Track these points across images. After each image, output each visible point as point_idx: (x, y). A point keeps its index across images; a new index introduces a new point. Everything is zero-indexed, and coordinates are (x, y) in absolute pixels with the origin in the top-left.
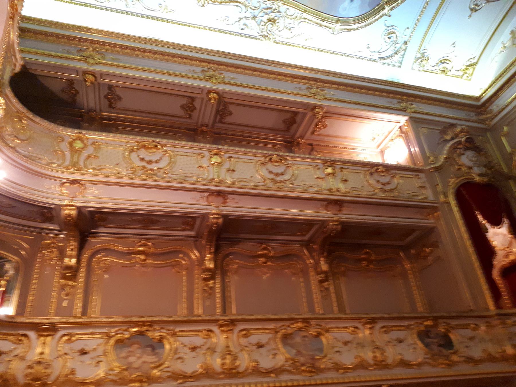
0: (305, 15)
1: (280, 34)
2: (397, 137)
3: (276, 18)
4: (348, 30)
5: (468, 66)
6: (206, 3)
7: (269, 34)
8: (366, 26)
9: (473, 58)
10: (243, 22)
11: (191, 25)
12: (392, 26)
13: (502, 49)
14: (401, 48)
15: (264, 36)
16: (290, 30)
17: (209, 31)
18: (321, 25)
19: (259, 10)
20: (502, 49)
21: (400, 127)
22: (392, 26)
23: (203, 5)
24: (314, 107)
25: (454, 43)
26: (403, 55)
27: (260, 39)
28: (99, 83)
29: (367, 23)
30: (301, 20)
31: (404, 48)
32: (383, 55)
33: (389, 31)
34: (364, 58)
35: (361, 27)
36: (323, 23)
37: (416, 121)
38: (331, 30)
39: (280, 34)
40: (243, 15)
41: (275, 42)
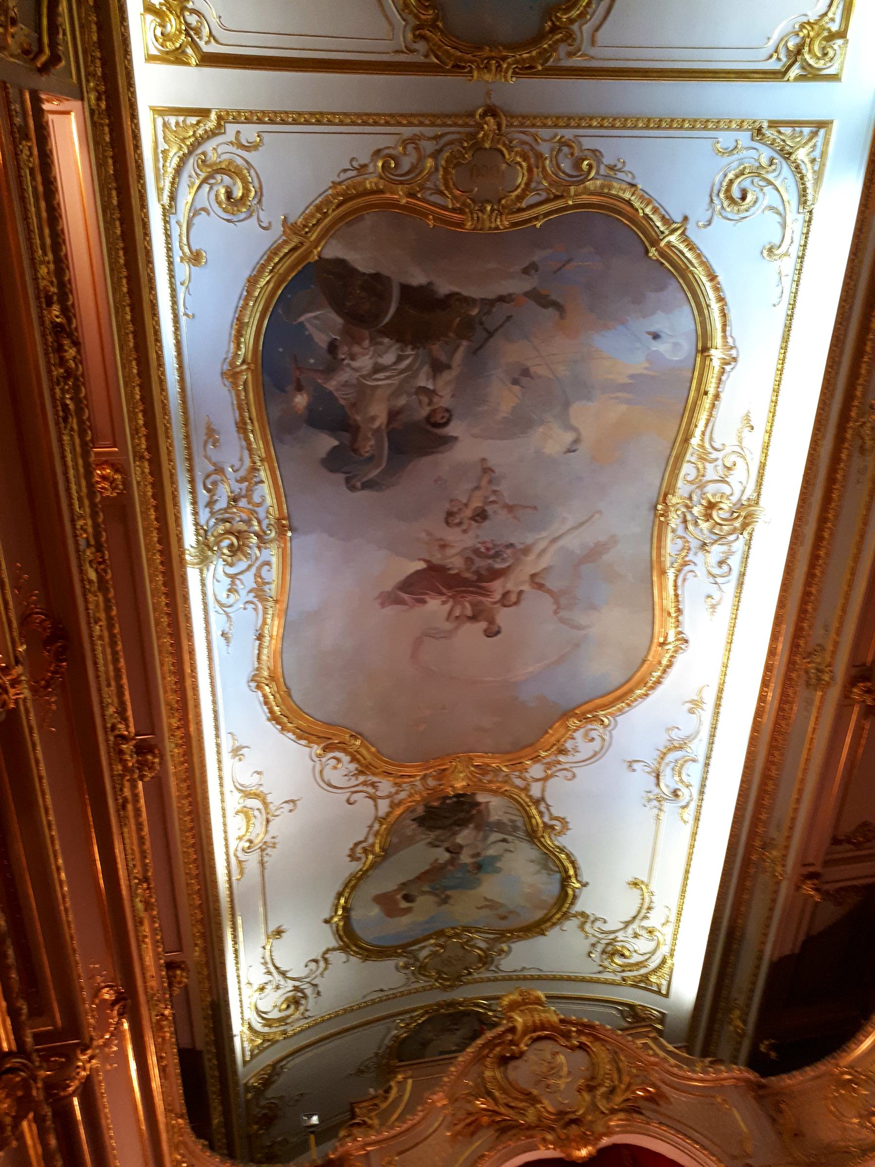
3: (704, 502)
4: (724, 325)
8: (712, 277)
11: (776, 391)
16: (729, 469)
18: (717, 397)
27: (751, 534)
28: (826, 863)
30: (707, 445)
33: (726, 203)
34: (694, 834)
35: (717, 289)
36: (712, 391)
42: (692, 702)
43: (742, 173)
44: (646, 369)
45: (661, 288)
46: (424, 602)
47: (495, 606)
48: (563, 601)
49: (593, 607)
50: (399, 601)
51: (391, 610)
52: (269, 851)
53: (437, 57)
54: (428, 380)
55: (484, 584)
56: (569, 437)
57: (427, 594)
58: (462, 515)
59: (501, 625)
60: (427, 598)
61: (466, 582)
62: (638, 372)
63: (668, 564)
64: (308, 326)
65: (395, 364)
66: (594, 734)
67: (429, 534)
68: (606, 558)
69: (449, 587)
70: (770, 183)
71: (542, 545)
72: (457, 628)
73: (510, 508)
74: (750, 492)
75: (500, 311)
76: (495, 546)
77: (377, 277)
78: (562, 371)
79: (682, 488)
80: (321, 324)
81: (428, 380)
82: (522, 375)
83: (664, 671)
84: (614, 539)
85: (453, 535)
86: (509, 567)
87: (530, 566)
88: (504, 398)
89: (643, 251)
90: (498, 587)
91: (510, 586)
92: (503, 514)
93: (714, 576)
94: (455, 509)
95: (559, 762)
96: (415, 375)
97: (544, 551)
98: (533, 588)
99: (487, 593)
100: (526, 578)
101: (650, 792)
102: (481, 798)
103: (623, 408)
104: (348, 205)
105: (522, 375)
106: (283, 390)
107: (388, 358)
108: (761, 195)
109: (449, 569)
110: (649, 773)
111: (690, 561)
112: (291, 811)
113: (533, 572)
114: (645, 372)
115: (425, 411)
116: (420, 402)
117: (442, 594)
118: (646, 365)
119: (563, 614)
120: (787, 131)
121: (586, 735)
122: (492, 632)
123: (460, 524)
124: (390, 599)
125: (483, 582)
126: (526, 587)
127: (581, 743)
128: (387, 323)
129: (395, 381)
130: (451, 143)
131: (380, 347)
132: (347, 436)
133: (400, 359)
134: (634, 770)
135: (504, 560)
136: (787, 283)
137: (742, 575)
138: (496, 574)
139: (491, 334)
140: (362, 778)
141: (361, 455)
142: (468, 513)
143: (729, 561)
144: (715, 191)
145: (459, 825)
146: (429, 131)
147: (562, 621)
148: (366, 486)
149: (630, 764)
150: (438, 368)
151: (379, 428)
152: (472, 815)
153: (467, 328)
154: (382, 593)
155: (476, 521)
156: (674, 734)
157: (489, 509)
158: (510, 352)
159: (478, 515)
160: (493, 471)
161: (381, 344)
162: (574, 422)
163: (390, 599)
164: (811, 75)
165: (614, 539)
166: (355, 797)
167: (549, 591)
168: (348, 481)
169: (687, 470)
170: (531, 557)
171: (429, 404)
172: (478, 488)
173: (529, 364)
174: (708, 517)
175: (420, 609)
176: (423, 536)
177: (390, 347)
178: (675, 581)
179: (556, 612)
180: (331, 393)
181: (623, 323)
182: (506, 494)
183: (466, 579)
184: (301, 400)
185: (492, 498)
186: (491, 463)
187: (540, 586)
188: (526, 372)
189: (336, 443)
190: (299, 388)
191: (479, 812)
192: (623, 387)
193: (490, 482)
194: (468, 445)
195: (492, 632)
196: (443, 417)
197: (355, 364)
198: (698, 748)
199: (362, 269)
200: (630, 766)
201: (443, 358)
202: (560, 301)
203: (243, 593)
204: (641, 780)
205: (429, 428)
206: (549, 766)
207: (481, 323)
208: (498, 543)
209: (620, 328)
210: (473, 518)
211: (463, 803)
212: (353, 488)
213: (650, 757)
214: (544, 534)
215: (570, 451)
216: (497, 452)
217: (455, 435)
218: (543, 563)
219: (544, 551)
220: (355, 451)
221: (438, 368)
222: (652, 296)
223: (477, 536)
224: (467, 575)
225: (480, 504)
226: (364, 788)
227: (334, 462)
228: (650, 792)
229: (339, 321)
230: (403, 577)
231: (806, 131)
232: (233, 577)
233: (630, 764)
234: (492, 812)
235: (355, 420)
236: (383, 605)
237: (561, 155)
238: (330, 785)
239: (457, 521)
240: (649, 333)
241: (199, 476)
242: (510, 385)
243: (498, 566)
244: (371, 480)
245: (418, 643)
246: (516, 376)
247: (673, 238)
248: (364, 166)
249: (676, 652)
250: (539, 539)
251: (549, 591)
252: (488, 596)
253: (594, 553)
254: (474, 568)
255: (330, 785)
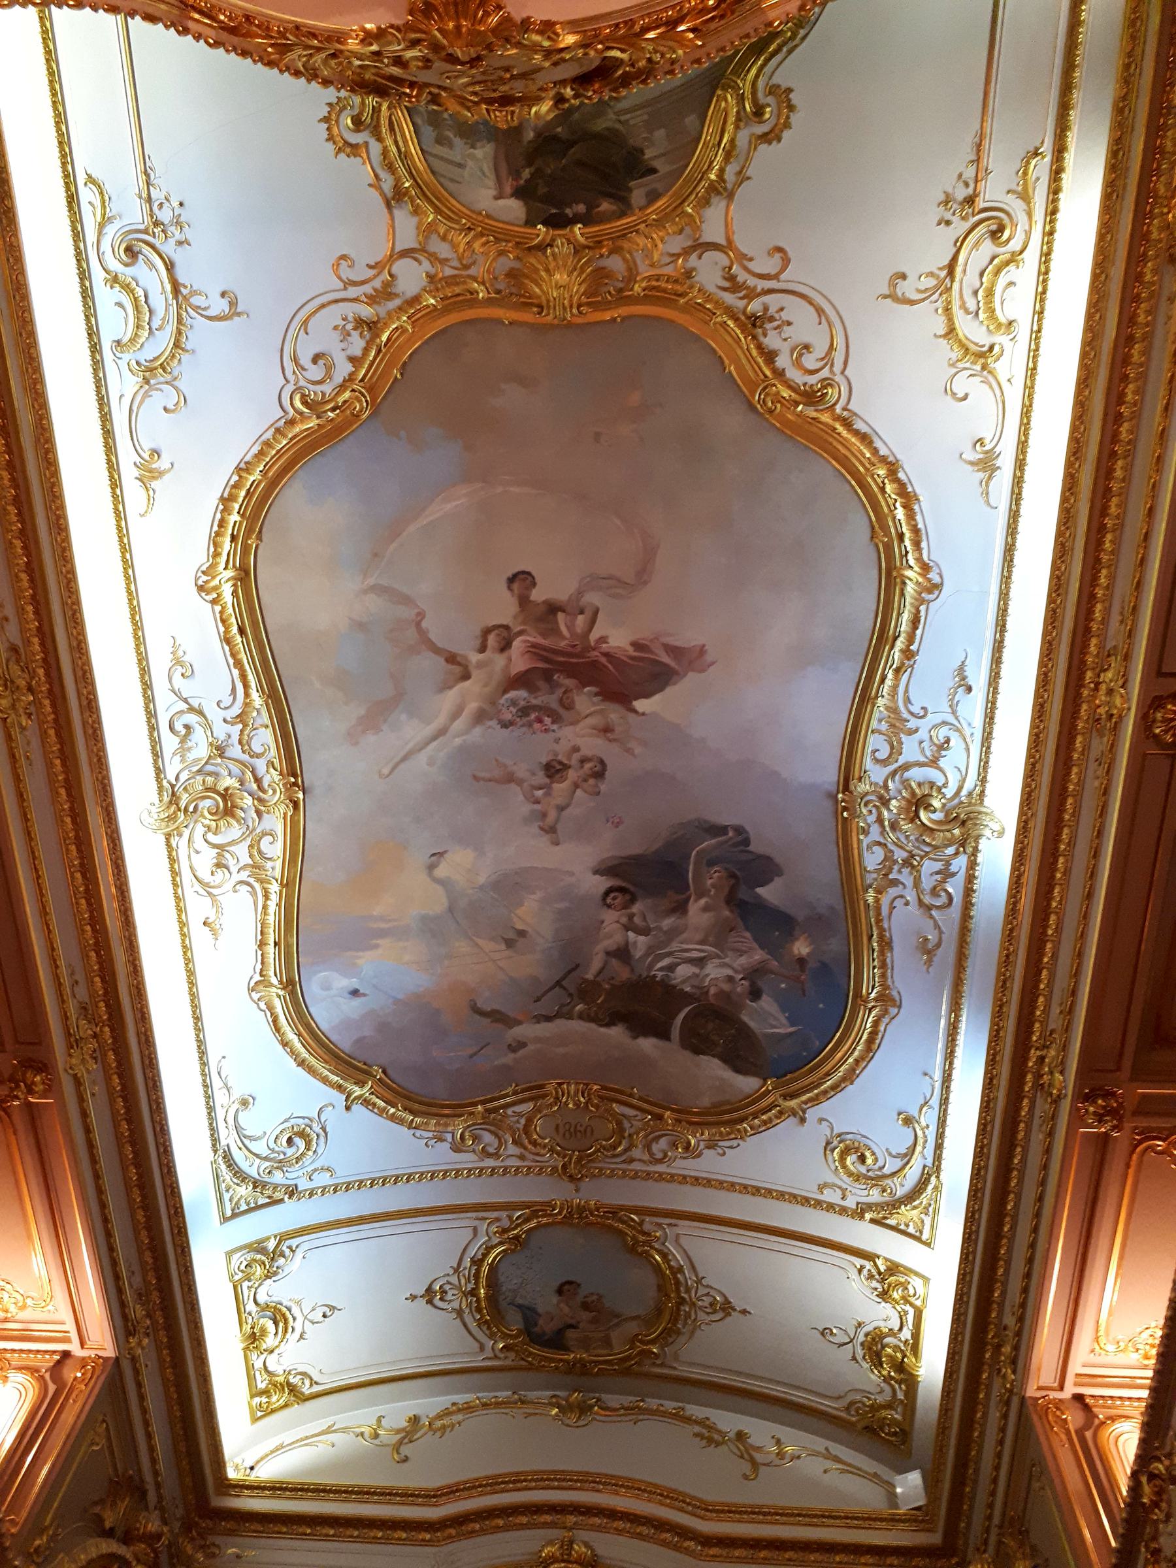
0: (274, 888)
1: (199, 843)
2: (33, 1370)
5: (289, 1384)
6: (209, 598)
7: (186, 810)
8: (301, 1063)
9: (313, 1383)
10: (192, 719)
12: (324, 1129)
13: (367, 1430)
14: (276, 1187)
15: (174, 798)
17: (129, 628)
18: (262, 944)
19: (245, 757)
20: (367, 1430)
21: (66, 1355)
22: (324, 1129)
23: (201, 589)
24: (44, 1066)
25: (333, 1308)
26: (258, 1207)
27: (160, 789)
29: (312, 1060)
30: (257, 886)
31: (278, 1195)
32: (239, 1156)
35: (293, 1053)
37: (115, 1379)
38: (257, 978)
39: (199, 843)
40: (215, 715)
41: (168, 837)
42: (159, 474)
43: (298, 1159)
44: (360, 957)
45: (359, 1041)
46: (636, 645)
47: (519, 629)
48: (411, 634)
49: (360, 626)
50: (675, 651)
51: (688, 638)
52: (961, 193)
53: (633, 1220)
54: (635, 943)
55: (541, 665)
56: (442, 871)
57: (632, 658)
58: (581, 772)
59: (507, 594)
60: (631, 651)
61: (570, 671)
62: (369, 953)
63: (264, 712)
64: (784, 1021)
65: (679, 964)
66: (315, 372)
67: (629, 751)
68: (357, 711)
69: (594, 664)
70: (266, 1159)
71: (459, 724)
72: (580, 593)
73: (510, 779)
74: (181, 844)
75: (548, 1005)
76: (530, 725)
77: (697, 1051)
78: (463, 946)
79: (275, 822)
80: (767, 1018)
81: (635, 943)
82: (514, 939)
83: (222, 523)
84: (352, 737)
85: (593, 745)
86: (505, 691)
87: (472, 692)
88: (532, 913)
89: (389, 1071)
90: (518, 660)
91: (500, 661)
92: (521, 771)
93: (192, 709)
94: (592, 781)
95: (372, 300)
96: (650, 950)
97: (455, 716)
98: (465, 658)
99: (534, 650)
100: (475, 673)
101: (180, 243)
102: (513, 209)
103: (377, 911)
104: (729, 1119)
105: (514, 939)
106: (824, 965)
107: (684, 971)
108: (272, 1145)
109: (596, 694)
110: (194, 293)
111: (236, 723)
112: (903, 277)
113: (467, 683)
114: (361, 954)
115: (636, 908)
116: (644, 919)
117: (606, 655)
118: (359, 962)
119: (408, 613)
120: (261, 1201)
121: (329, 368)
122: (521, 580)
123: (583, 761)
124: (690, 659)
125: (546, 669)
126: (474, 657)
127: (333, 342)
128: (687, 1006)
129: (675, 946)
130: (614, 1156)
131: (696, 983)
132: (743, 894)
133: (671, 968)
134: (223, 294)
135: (514, 703)
136: (217, 1083)
137: (153, 728)
138: (521, 681)
139: (558, 983)
140: (755, 306)
141: (726, 869)
142: (572, 775)
143: (177, 740)
144: (322, 1139)
145: (555, 138)
146: (636, 1166)
147: (406, 600)
148: (722, 830)
149: (234, 311)
150: (622, 953)
151: (699, 897)
152: (530, 165)
153: (586, 991)
154: (703, 671)
155: (560, 763)
156: (169, 397)
157: (541, 778)
158: (530, 965)
159: (558, 771)
160: (542, 829)
161: (693, 986)
162: (440, 889)
163: (690, 659)
164: (258, 1247)
165: (352, 737)
166: (769, 265)
167: (437, 650)
168: (746, 842)
169: (275, 849)
170: (472, 706)
171: (633, 915)
172: (561, 809)
173: (507, 953)
174: (226, 795)
175: (643, 633)
176: (638, 750)
177: (684, 982)
178: (246, 686)
179: (421, 615)
180: (762, 948)
181: (397, 1002)
182: (521, 797)
183: (569, 676)
184: (801, 948)
185: (539, 793)
186: (545, 839)
187: (452, 659)
188: (510, 943)
189: (759, 890)
190: (801, 961)
191: (515, 173)
192: (382, 934)
193: (544, 815)
194: (578, 865)
195: (521, 580)
196: (614, 898)
197: (730, 972)
198: (122, 383)
199: (716, 1061)
200: (233, 304)
201: (614, 962)
202: (477, 1017)
203: (923, 734)
204: (204, 271)
205: (632, 888)
206: (386, 293)
207: (570, 995)
208: (524, 729)
209: (401, 996)
210: (566, 767)
211: (548, 199)
212: (739, 830)
213: (200, 332)
214: (458, 741)
215: (440, 854)
216: (535, 851)
217: (597, 876)
218: (452, 696)
219: (455, 716)
220: (732, 875)
221: (622, 953)
222: (367, 1032)
223: (557, 741)
224: (569, 682)
225: (556, 786)
226: (752, 281)
227: (765, 868)
228: (180, 243)
229: (745, 1018)
230: (669, 690)
231: (244, 1207)
232: (934, 762)
233: (234, 311)
234: (487, 167)
235: (732, 911)
236: (702, 650)
237: (496, 1145)
238: (820, 311)
239: (588, 766)
240: (364, 995)
241: (956, 910)
242: (529, 930)
243: (520, 694)
244: (716, 835)
245: (643, 574)
246: (522, 940)
247: (358, 1091)
248: (708, 1147)
249: (213, 566)
250: (463, 733)
251: (437, 650)
252: (534, 645)
253: (376, 716)
254: (559, 692)
255: (820, 311)
